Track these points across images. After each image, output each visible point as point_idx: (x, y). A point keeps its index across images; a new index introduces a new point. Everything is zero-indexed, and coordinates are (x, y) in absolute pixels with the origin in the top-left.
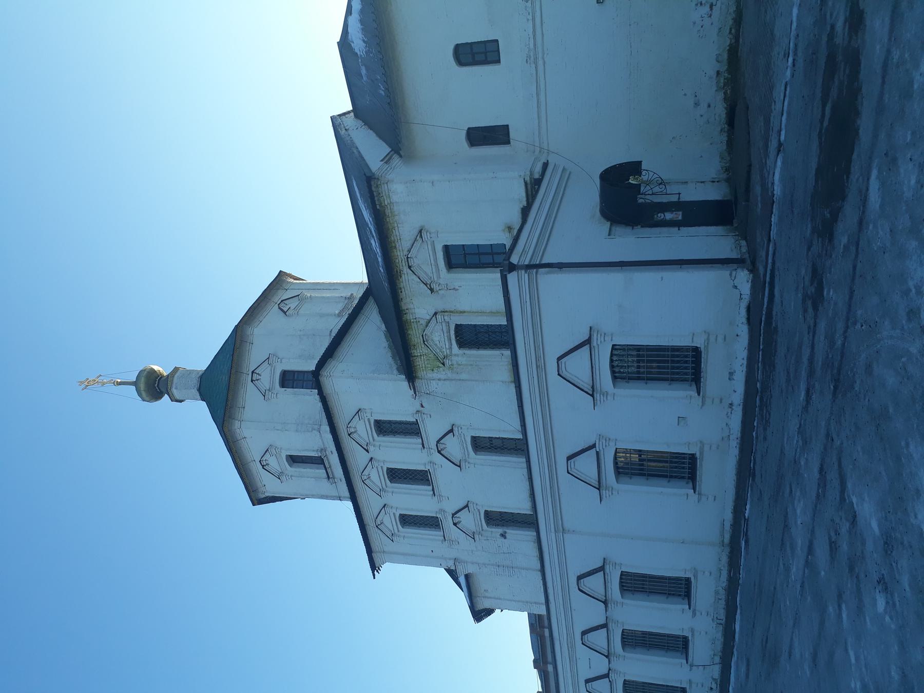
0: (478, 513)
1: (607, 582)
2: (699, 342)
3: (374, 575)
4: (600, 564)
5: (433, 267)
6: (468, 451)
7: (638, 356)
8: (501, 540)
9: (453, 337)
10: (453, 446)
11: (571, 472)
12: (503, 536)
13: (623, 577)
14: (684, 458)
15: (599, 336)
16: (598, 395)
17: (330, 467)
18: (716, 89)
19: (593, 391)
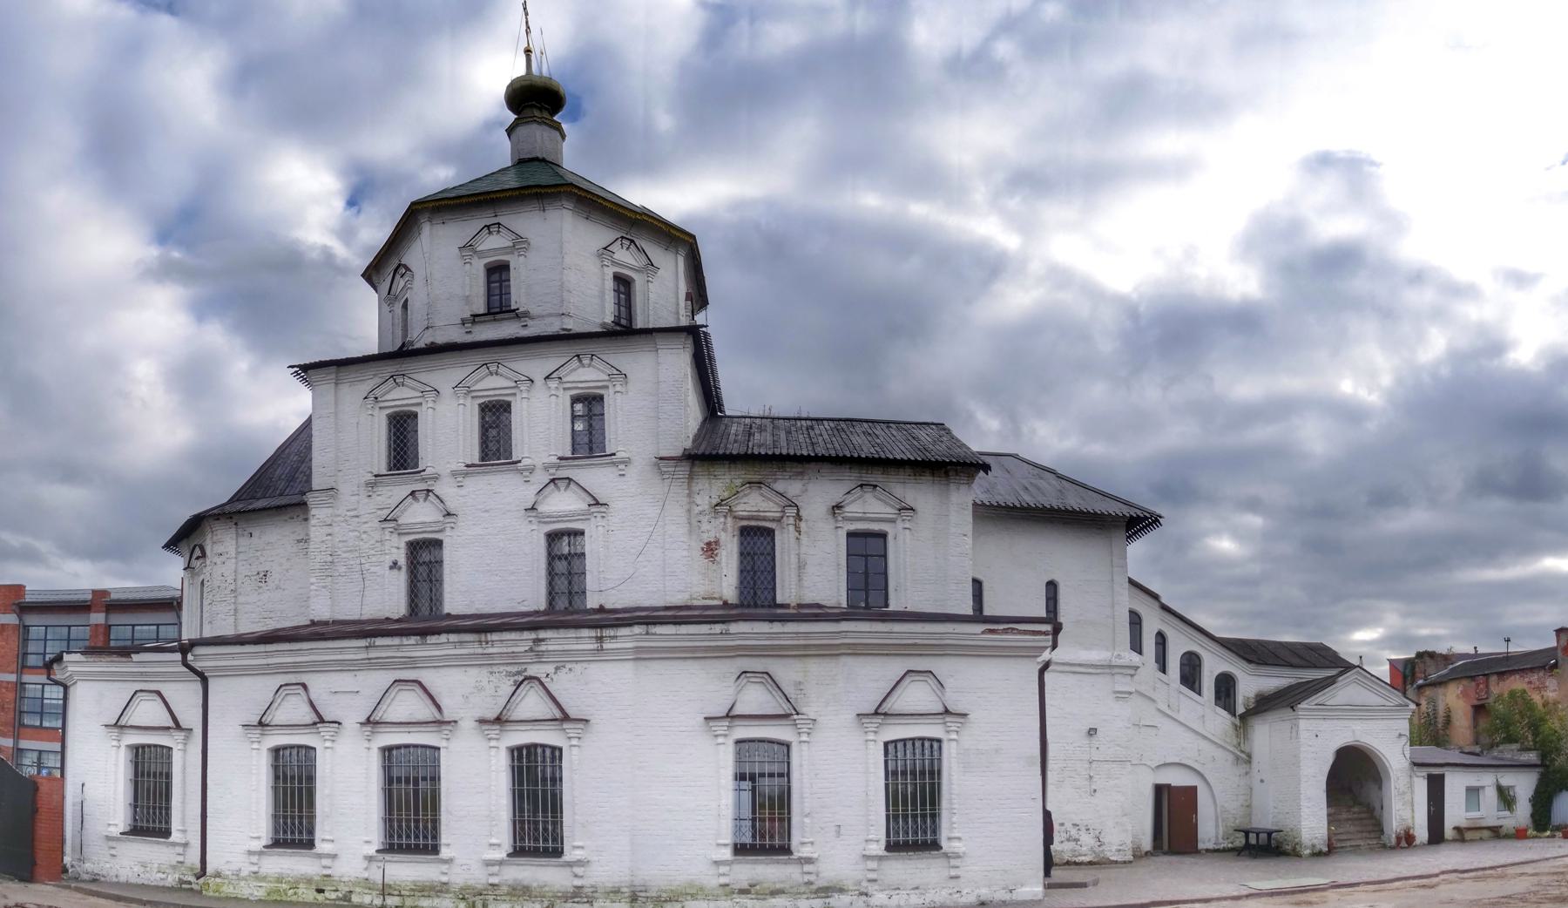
0: (437, 529)
2: (445, 853)
3: (292, 367)
4: (572, 713)
7: (161, 774)
8: (388, 560)
9: (753, 523)
11: (281, 690)
12: (395, 565)
13: (152, 749)
15: (332, 733)
16: (727, 724)
17: (495, 320)
18: (511, 851)
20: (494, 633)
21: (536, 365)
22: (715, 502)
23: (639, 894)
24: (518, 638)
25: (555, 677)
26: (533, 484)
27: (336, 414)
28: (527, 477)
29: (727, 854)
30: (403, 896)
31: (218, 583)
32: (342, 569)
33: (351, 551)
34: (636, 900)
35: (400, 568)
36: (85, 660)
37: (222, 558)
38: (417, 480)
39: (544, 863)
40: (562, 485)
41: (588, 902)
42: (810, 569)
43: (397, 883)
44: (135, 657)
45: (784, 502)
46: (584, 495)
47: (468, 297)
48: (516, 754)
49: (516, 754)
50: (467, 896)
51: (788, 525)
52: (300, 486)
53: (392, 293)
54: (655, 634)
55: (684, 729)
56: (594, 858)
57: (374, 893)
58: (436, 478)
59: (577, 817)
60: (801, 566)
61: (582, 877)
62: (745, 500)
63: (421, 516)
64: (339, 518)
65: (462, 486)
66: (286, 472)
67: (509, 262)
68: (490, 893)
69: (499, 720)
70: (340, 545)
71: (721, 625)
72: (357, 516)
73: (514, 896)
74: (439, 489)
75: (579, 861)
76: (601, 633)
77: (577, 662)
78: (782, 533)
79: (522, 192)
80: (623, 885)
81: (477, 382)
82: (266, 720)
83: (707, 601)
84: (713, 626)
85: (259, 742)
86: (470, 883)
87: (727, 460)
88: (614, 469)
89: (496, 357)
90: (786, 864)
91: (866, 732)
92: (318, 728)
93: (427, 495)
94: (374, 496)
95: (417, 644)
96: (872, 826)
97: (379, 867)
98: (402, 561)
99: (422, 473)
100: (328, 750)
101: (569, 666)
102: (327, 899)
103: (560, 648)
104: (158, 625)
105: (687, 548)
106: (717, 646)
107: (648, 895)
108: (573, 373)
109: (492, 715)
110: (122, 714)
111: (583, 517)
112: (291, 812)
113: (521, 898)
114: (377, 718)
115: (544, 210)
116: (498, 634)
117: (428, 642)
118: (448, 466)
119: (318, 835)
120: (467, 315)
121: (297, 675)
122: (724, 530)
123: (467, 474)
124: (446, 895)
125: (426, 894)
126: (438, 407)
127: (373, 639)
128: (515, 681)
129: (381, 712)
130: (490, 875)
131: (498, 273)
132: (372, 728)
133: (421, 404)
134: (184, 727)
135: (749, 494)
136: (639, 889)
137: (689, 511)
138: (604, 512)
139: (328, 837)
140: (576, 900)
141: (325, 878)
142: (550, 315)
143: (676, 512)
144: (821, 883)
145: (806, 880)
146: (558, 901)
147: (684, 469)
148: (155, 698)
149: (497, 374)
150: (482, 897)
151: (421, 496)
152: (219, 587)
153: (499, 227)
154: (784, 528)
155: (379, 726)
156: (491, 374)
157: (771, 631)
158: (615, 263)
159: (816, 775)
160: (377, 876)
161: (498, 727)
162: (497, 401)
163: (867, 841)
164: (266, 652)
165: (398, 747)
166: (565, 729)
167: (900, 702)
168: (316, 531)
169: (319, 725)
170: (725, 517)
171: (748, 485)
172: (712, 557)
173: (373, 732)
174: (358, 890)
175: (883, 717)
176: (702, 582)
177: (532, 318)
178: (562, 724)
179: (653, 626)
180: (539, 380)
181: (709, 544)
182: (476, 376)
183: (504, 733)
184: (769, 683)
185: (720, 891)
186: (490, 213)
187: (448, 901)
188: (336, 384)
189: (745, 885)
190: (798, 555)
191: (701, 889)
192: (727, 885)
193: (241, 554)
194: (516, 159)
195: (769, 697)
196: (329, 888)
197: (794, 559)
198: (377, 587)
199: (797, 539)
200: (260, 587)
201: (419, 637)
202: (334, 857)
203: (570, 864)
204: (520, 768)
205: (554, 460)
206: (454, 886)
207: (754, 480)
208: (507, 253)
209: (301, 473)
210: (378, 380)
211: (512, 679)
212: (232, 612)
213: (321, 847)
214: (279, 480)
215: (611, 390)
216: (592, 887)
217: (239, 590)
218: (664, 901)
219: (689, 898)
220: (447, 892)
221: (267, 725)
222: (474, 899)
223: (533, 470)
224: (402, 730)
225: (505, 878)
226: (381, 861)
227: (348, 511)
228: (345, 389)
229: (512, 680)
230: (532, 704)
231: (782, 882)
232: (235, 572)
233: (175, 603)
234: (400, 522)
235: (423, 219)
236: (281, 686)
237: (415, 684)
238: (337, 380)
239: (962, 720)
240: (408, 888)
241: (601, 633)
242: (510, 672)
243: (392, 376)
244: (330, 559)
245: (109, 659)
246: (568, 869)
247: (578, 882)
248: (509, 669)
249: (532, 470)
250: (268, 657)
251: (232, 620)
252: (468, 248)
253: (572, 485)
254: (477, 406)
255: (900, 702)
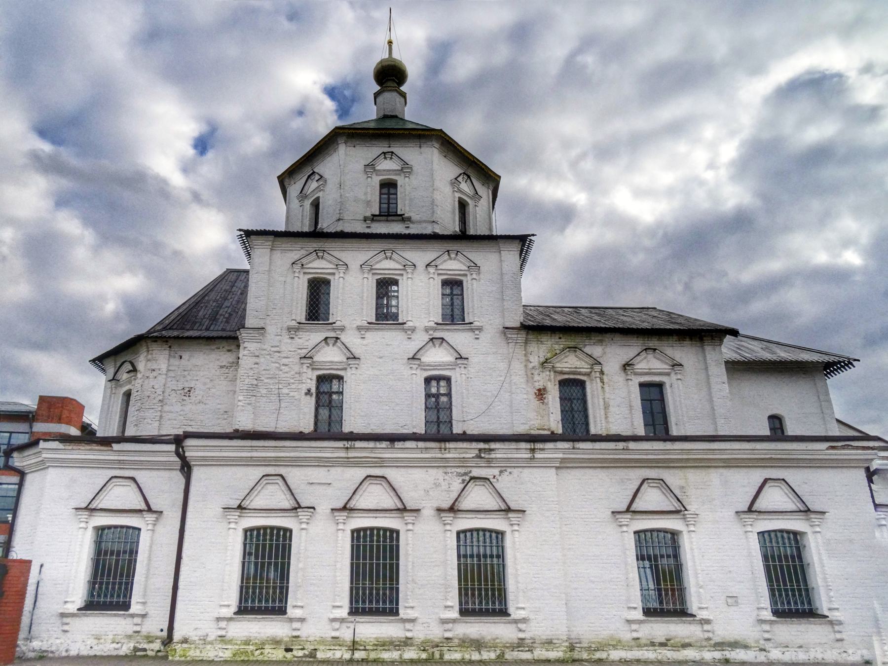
1: (487, 513)
3: (240, 230)
4: (513, 506)
5: (647, 371)
6: (429, 370)
9: (572, 377)
10: (437, 356)
12: (308, 393)
14: (125, 596)
17: (387, 220)
19: (634, 512)
20: (450, 443)
21: (420, 256)
22: (542, 360)
23: (575, 645)
24: (468, 447)
25: (500, 478)
26: (414, 340)
27: (269, 271)
28: (410, 335)
29: (638, 615)
30: (368, 650)
31: (148, 394)
32: (264, 391)
33: (270, 378)
34: (574, 649)
35: (311, 395)
36: (63, 448)
37: (155, 374)
38: (329, 330)
39: (496, 621)
40: (437, 342)
41: (529, 651)
42: (611, 409)
43: (363, 639)
44: (116, 447)
45: (591, 361)
46: (452, 351)
47: (369, 201)
48: (355, 535)
49: (355, 535)
50: (427, 648)
51: (596, 377)
52: (222, 325)
53: (303, 192)
54: (579, 449)
55: (598, 520)
56: (532, 617)
57: (344, 648)
58: (342, 329)
59: (520, 585)
60: (606, 407)
61: (524, 631)
62: (566, 360)
63: (331, 356)
64: (264, 352)
65: (364, 338)
66: (208, 313)
67: (397, 180)
68: (445, 645)
69: (452, 509)
70: (264, 372)
71: (623, 443)
72: (279, 352)
73: (464, 647)
74: (343, 337)
75: (524, 619)
76: (534, 445)
77: (514, 467)
78: (592, 383)
79: (411, 132)
80: (553, 637)
81: (377, 263)
82: (245, 504)
83: (540, 431)
84: (617, 443)
85: (413, 524)
86: (429, 637)
87: (549, 331)
88: (470, 334)
89: (391, 246)
90: (690, 623)
91: (744, 526)
92: (298, 512)
93: (336, 342)
94: (296, 338)
95: (388, 448)
96: (762, 597)
97: (348, 627)
98: (313, 390)
99: (334, 325)
100: (304, 531)
101: (509, 470)
102: (295, 657)
103: (505, 456)
104: (11, 433)
105: (526, 392)
106: (620, 459)
107: (582, 645)
108: (444, 264)
109: (446, 505)
110: (94, 498)
111: (451, 367)
112: (363, 584)
113: (469, 649)
114: (352, 506)
115: (420, 147)
116: (455, 443)
117: (396, 446)
118: (354, 322)
119: (291, 602)
120: (368, 214)
121: (276, 468)
122: (550, 380)
123: (368, 329)
124: (411, 648)
125: (386, 648)
126: (347, 277)
127: (353, 442)
128: (463, 481)
129: (249, 502)
130: (445, 631)
131: (388, 187)
132: (348, 513)
133: (334, 274)
134: (153, 510)
135: (568, 356)
136: (575, 641)
137: (526, 366)
138: (466, 364)
139: (299, 604)
140: (520, 649)
141: (294, 639)
142: (425, 221)
143: (518, 367)
144: (717, 639)
145: (706, 637)
146: (507, 650)
147: (522, 336)
148: (129, 484)
149: (391, 258)
150: (439, 648)
151: (331, 342)
152: (149, 397)
153: (392, 155)
154: (593, 380)
155: (353, 512)
156: (387, 258)
157: (665, 448)
158: (460, 191)
159: (703, 556)
160: (346, 634)
161: (452, 515)
162: (390, 278)
163: (758, 609)
164: (251, 447)
165: (109, 527)
166: (509, 518)
167: (363, 501)
168: (246, 361)
169: (298, 510)
170: (550, 371)
171: (568, 349)
172: (542, 400)
173: (90, 516)
174: (322, 647)
175: (757, 514)
176: (536, 417)
177: (412, 222)
178: (507, 514)
179: (577, 443)
180: (421, 266)
181: (539, 390)
182: (377, 259)
183: (350, 519)
184: (663, 486)
185: (633, 643)
186: (386, 144)
187: (413, 652)
188: (271, 250)
189: (663, 640)
190: (604, 399)
191: (620, 641)
192: (638, 639)
193: (171, 372)
194: (381, 114)
195: (663, 497)
196: (296, 647)
197: (602, 403)
198: (294, 408)
199: (602, 388)
200: (183, 400)
201: (388, 443)
202: (302, 620)
203: (516, 622)
204: (358, 547)
205: (432, 324)
206: (417, 640)
207: (571, 346)
208: (396, 175)
209: (221, 315)
210: (303, 252)
211: (461, 478)
212: (158, 418)
213: (291, 612)
214: (204, 318)
215: (469, 277)
216: (532, 638)
217: (165, 400)
218: (594, 650)
219: (611, 648)
220: (412, 645)
221: (245, 509)
222: (432, 650)
223: (414, 330)
224: (387, 515)
225: (456, 633)
226: (352, 622)
227: (272, 347)
228: (277, 255)
229: (461, 480)
230: (478, 497)
231: (688, 637)
232: (164, 385)
233: (31, 416)
234: (315, 359)
235: (341, 140)
236: (264, 476)
237: (382, 479)
238: (272, 247)
239: (821, 517)
240: (371, 644)
241: (534, 445)
242: (460, 473)
243: (315, 251)
244: (255, 382)
245: (88, 447)
246: (514, 625)
247: (521, 635)
248: (459, 470)
249: (413, 330)
250: (252, 451)
251: (156, 424)
252: (370, 167)
253: (444, 344)
254: (375, 281)
255: (363, 501)
